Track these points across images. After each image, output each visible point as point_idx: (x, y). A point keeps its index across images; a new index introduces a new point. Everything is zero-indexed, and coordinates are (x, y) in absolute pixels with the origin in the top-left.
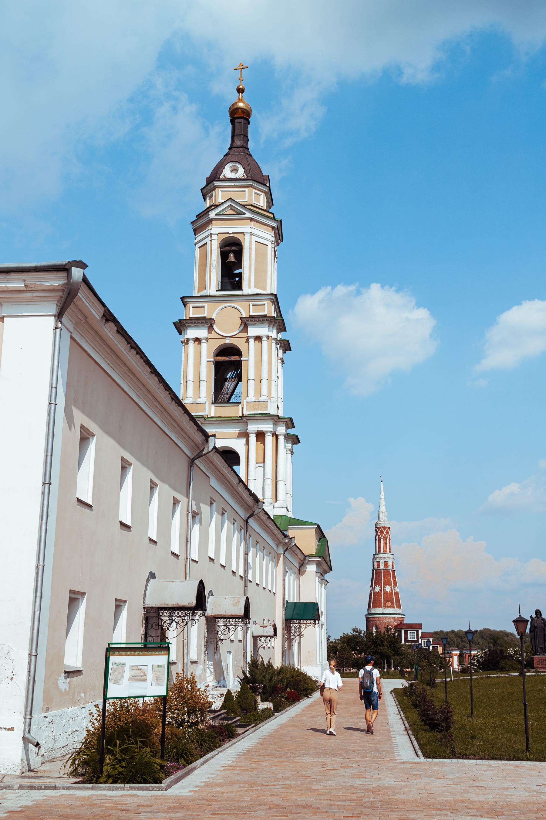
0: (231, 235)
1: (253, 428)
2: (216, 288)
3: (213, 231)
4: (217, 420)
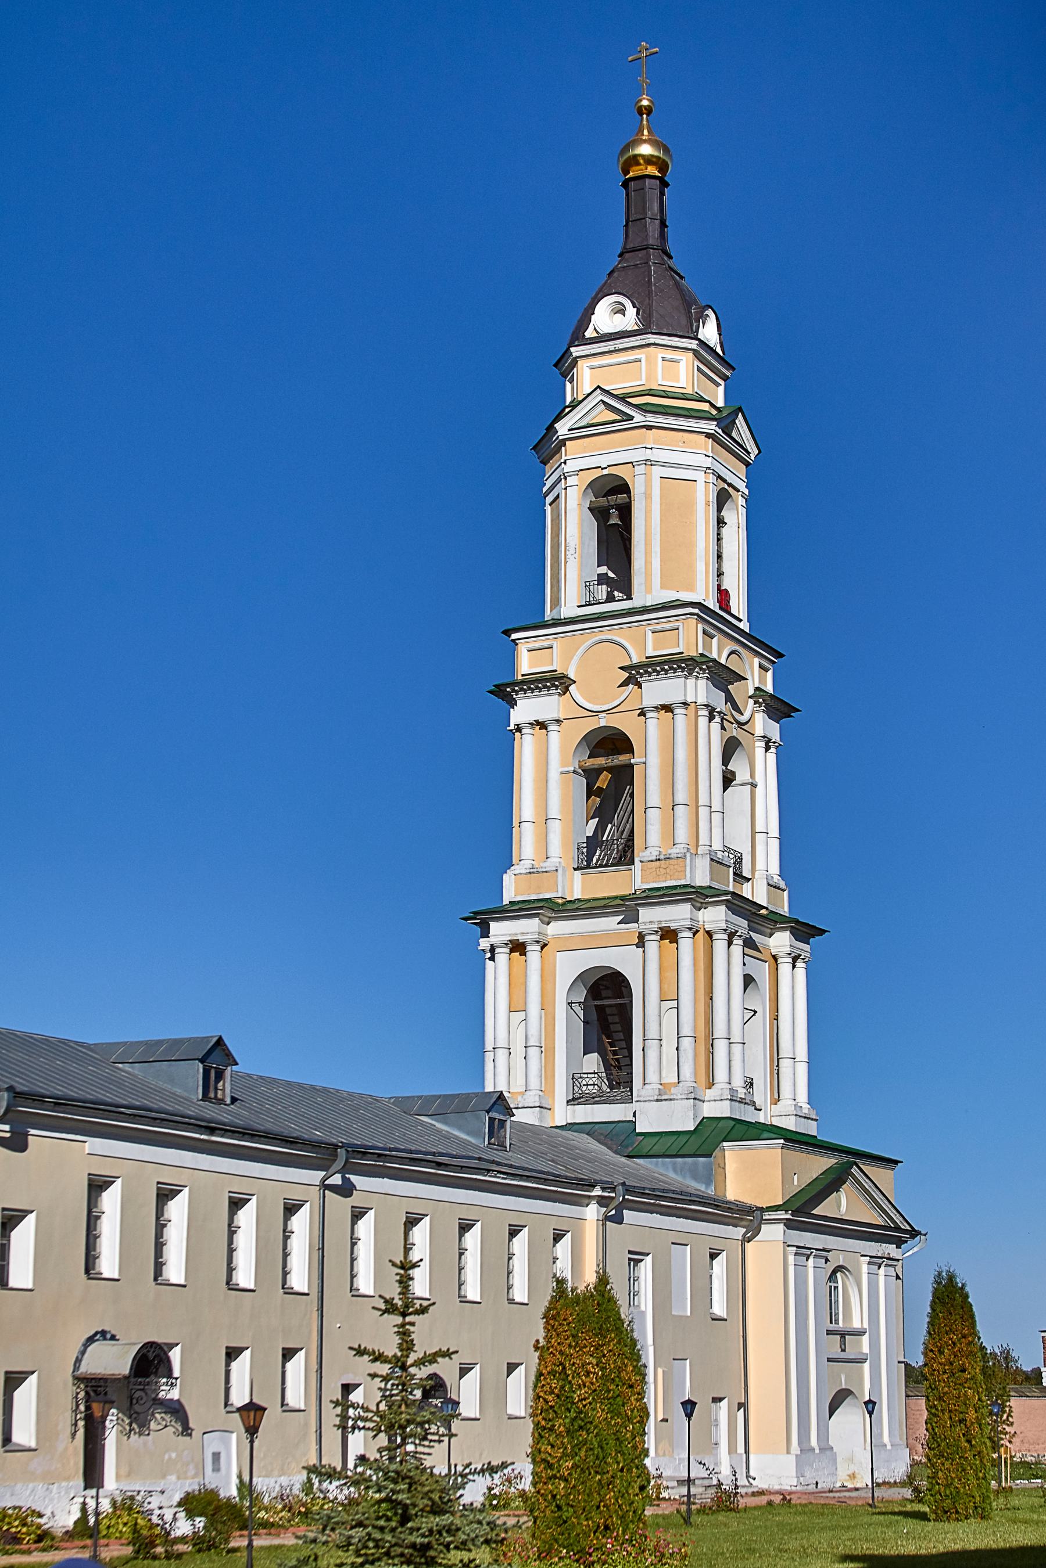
0: (605, 472)
1: (651, 916)
2: (579, 601)
3: (566, 468)
4: (577, 909)
